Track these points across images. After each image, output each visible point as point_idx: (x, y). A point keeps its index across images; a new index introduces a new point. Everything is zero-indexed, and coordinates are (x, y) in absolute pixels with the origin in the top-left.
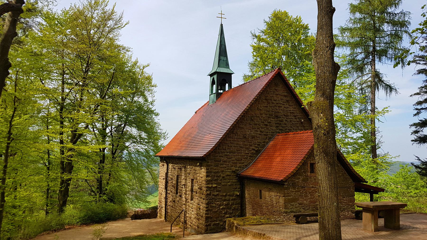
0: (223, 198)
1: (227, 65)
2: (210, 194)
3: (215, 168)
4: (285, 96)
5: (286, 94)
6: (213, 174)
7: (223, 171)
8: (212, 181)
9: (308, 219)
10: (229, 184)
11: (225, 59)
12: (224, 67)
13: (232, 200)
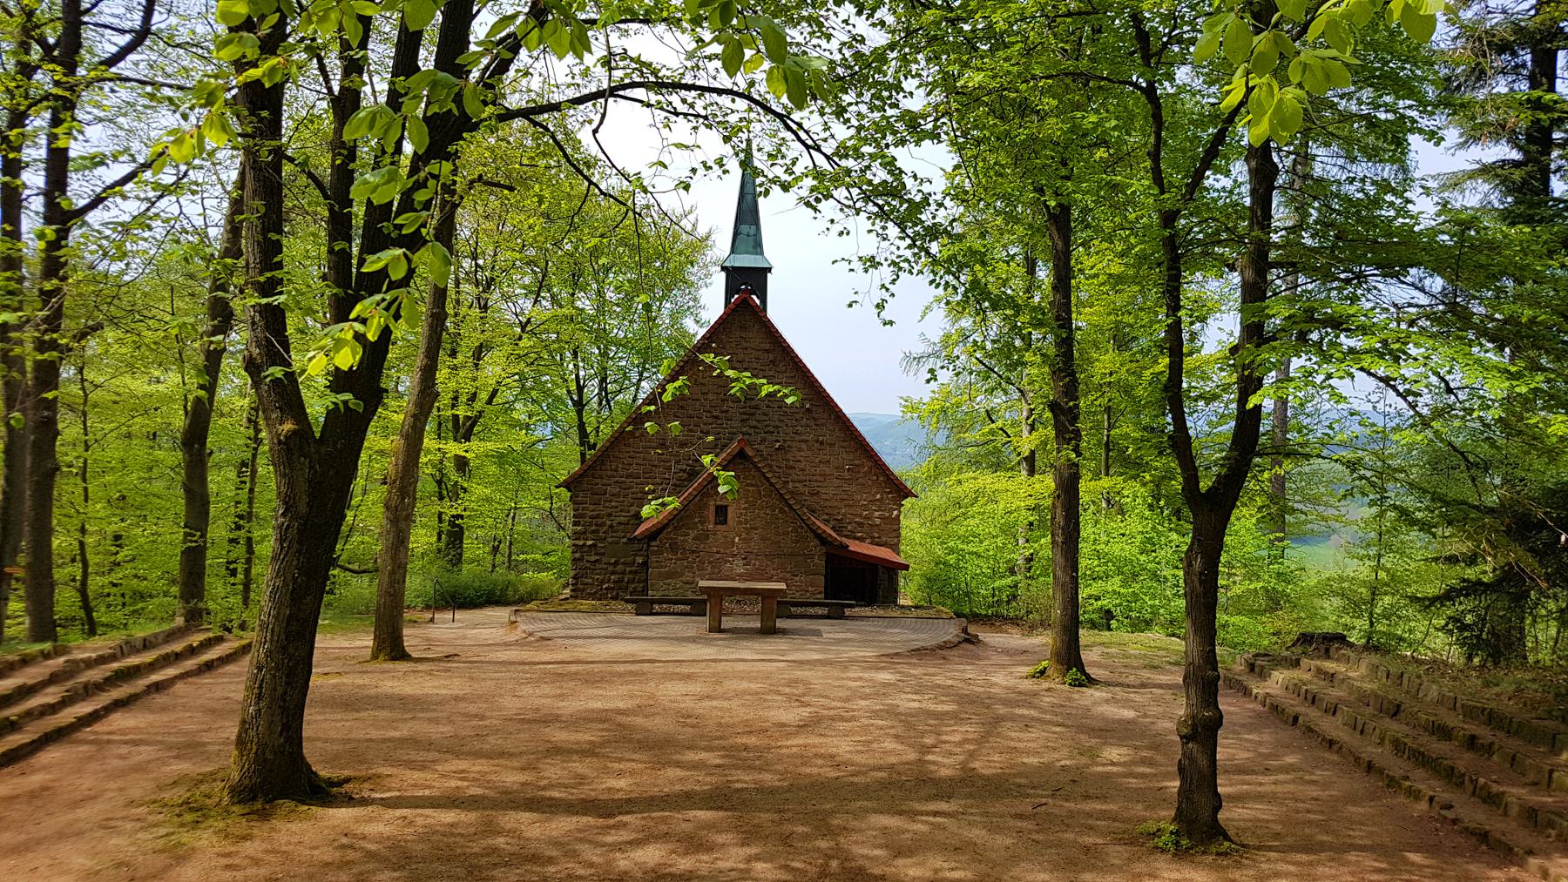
0: (611, 568)
1: (757, 247)
2: (581, 559)
3: (592, 507)
4: (768, 351)
5: (767, 346)
6: (588, 519)
7: (610, 515)
8: (585, 533)
9: (656, 607)
10: (624, 540)
11: (752, 230)
12: (748, 253)
13: (630, 572)
